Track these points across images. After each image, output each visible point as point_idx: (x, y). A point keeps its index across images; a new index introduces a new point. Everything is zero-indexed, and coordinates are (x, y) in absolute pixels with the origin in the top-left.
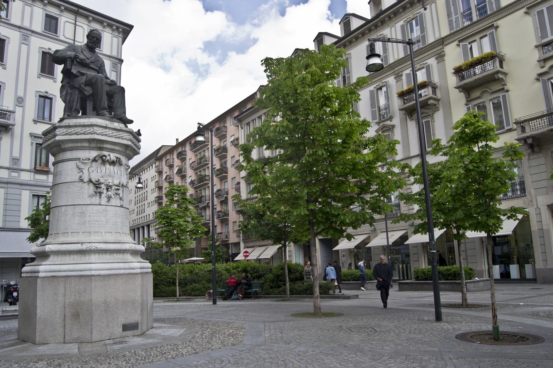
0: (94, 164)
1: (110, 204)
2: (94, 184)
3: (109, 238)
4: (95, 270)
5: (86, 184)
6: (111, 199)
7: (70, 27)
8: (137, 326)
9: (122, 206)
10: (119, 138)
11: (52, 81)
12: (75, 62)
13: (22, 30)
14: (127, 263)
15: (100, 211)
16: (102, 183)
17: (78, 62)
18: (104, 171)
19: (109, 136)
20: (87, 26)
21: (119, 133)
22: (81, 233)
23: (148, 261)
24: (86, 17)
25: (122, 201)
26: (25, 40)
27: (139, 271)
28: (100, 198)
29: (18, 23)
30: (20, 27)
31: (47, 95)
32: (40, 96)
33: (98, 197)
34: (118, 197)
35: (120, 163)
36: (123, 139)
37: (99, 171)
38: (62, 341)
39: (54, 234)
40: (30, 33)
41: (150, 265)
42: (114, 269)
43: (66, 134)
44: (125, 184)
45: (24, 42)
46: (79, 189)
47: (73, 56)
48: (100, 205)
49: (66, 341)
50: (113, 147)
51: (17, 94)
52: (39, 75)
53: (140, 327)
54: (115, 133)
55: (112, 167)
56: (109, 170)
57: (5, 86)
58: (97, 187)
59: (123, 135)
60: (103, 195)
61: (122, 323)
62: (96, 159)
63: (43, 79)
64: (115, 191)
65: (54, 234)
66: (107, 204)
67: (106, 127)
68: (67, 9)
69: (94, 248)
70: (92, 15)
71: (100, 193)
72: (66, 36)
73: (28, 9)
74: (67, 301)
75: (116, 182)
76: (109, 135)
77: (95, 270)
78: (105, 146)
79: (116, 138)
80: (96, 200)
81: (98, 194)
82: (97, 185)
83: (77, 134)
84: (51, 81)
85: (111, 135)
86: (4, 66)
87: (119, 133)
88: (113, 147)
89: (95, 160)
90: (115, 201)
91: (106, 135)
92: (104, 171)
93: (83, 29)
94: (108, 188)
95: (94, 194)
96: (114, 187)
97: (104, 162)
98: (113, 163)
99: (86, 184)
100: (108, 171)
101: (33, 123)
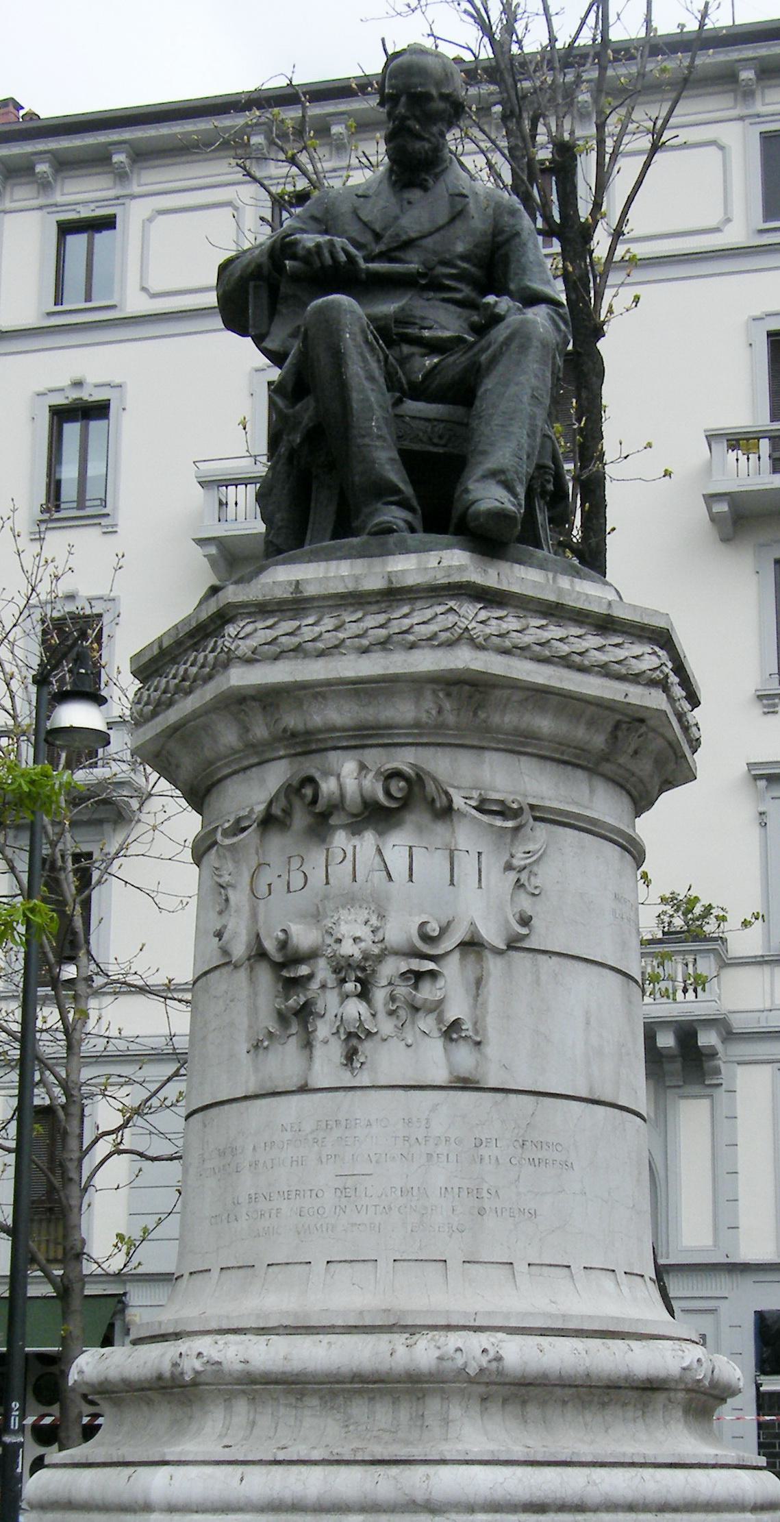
0: (277, 843)
1: (364, 1079)
2: (278, 967)
5: (242, 974)
6: (366, 1048)
9: (465, 1084)
10: (384, 644)
12: (284, 289)
14: (394, 1471)
15: (308, 1127)
17: (295, 278)
18: (317, 877)
19: (321, 654)
20: (737, 127)
22: (384, 1265)
24: (725, 79)
33: (292, 1045)
34: (427, 1023)
36: (412, 646)
37: (297, 881)
39: (215, 1272)
44: (492, 935)
47: (265, 259)
48: (304, 1089)
55: (368, 840)
56: (348, 863)
59: (407, 623)
60: (323, 1029)
62: (277, 811)
65: (215, 1272)
66: (346, 1079)
69: (198, 1365)
70: (749, 53)
71: (305, 1013)
75: (400, 930)
76: (320, 645)
79: (365, 651)
85: (330, 639)
89: (269, 822)
91: (298, 650)
92: (317, 877)
93: (722, 148)
96: (390, 968)
99: (242, 975)
100: (341, 873)
101: (757, 710)
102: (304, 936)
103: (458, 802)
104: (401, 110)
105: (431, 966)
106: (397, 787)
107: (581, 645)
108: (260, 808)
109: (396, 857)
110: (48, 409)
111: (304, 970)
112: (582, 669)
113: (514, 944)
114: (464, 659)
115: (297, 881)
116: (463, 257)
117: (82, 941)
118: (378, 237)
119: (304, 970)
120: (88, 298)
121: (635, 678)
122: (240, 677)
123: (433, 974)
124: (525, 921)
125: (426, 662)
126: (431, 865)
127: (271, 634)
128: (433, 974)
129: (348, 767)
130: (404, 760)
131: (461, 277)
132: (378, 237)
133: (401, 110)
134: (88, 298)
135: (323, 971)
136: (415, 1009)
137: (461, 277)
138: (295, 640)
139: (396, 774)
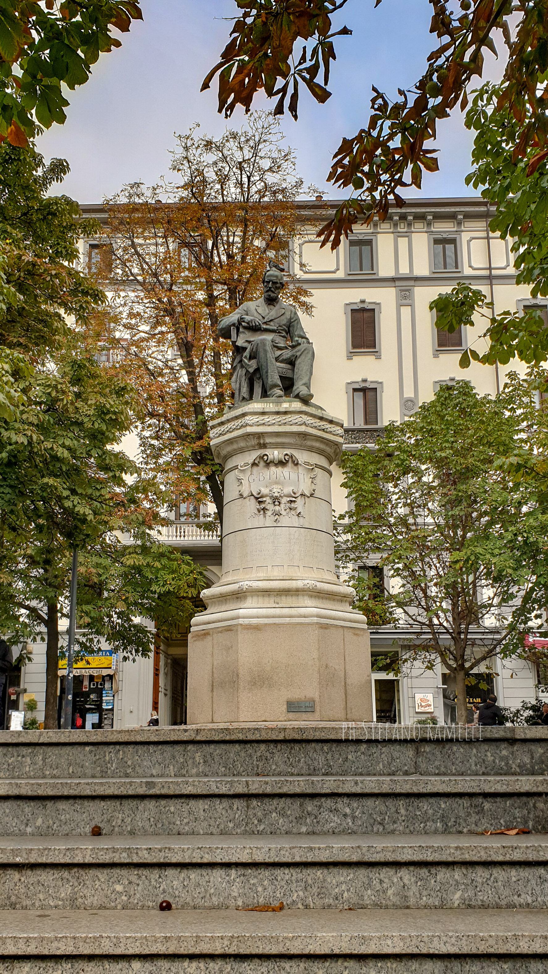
0: (255, 469)
2: (257, 498)
3: (276, 573)
4: (244, 618)
7: (478, 246)
8: (313, 707)
11: (374, 357)
13: (398, 283)
16: (266, 496)
17: (245, 328)
19: (269, 425)
21: (284, 418)
23: (361, 612)
25: (301, 519)
26: (405, 298)
27: (315, 620)
28: (265, 517)
29: (391, 273)
30: (393, 280)
31: (367, 385)
32: (355, 390)
34: (293, 512)
35: (293, 462)
37: (262, 478)
38: (211, 720)
40: (412, 283)
41: (364, 618)
42: (273, 617)
43: (221, 435)
45: (404, 302)
46: (239, 508)
49: (215, 720)
50: (279, 440)
51: (403, 395)
52: (350, 355)
53: (318, 709)
54: (278, 418)
57: (382, 387)
58: (260, 502)
59: (290, 419)
61: (285, 699)
62: (256, 462)
63: (358, 360)
64: (289, 505)
67: (263, 413)
68: (468, 216)
72: (475, 266)
73: (403, 242)
74: (215, 664)
77: (244, 618)
78: (268, 440)
79: (280, 425)
80: (259, 520)
81: (262, 512)
82: (259, 499)
83: (231, 432)
84: (371, 359)
86: (378, 354)
87: (284, 418)
88: (279, 440)
89: (254, 464)
90: (288, 519)
94: (276, 500)
95: (257, 512)
97: (268, 464)
98: (282, 463)
102: (265, 491)
103: (300, 462)
104: (270, 285)
105: (294, 499)
106: (287, 457)
107: (327, 427)
108: (252, 461)
109: (286, 474)
110: (382, 357)
111: (264, 499)
112: (327, 432)
113: (312, 495)
114: (303, 429)
115: (262, 478)
116: (284, 325)
117: (429, 716)
118: (264, 318)
119: (264, 499)
120: (445, 268)
121: (337, 435)
122: (249, 429)
123: (294, 501)
124: (314, 491)
125: (295, 429)
126: (294, 476)
127: (258, 420)
128: (294, 501)
129: (276, 452)
130: (288, 451)
131: (284, 330)
132: (264, 318)
133: (270, 285)
134: (445, 268)
135: (268, 500)
136: (291, 509)
137: (284, 330)
138: (263, 422)
139: (286, 455)
